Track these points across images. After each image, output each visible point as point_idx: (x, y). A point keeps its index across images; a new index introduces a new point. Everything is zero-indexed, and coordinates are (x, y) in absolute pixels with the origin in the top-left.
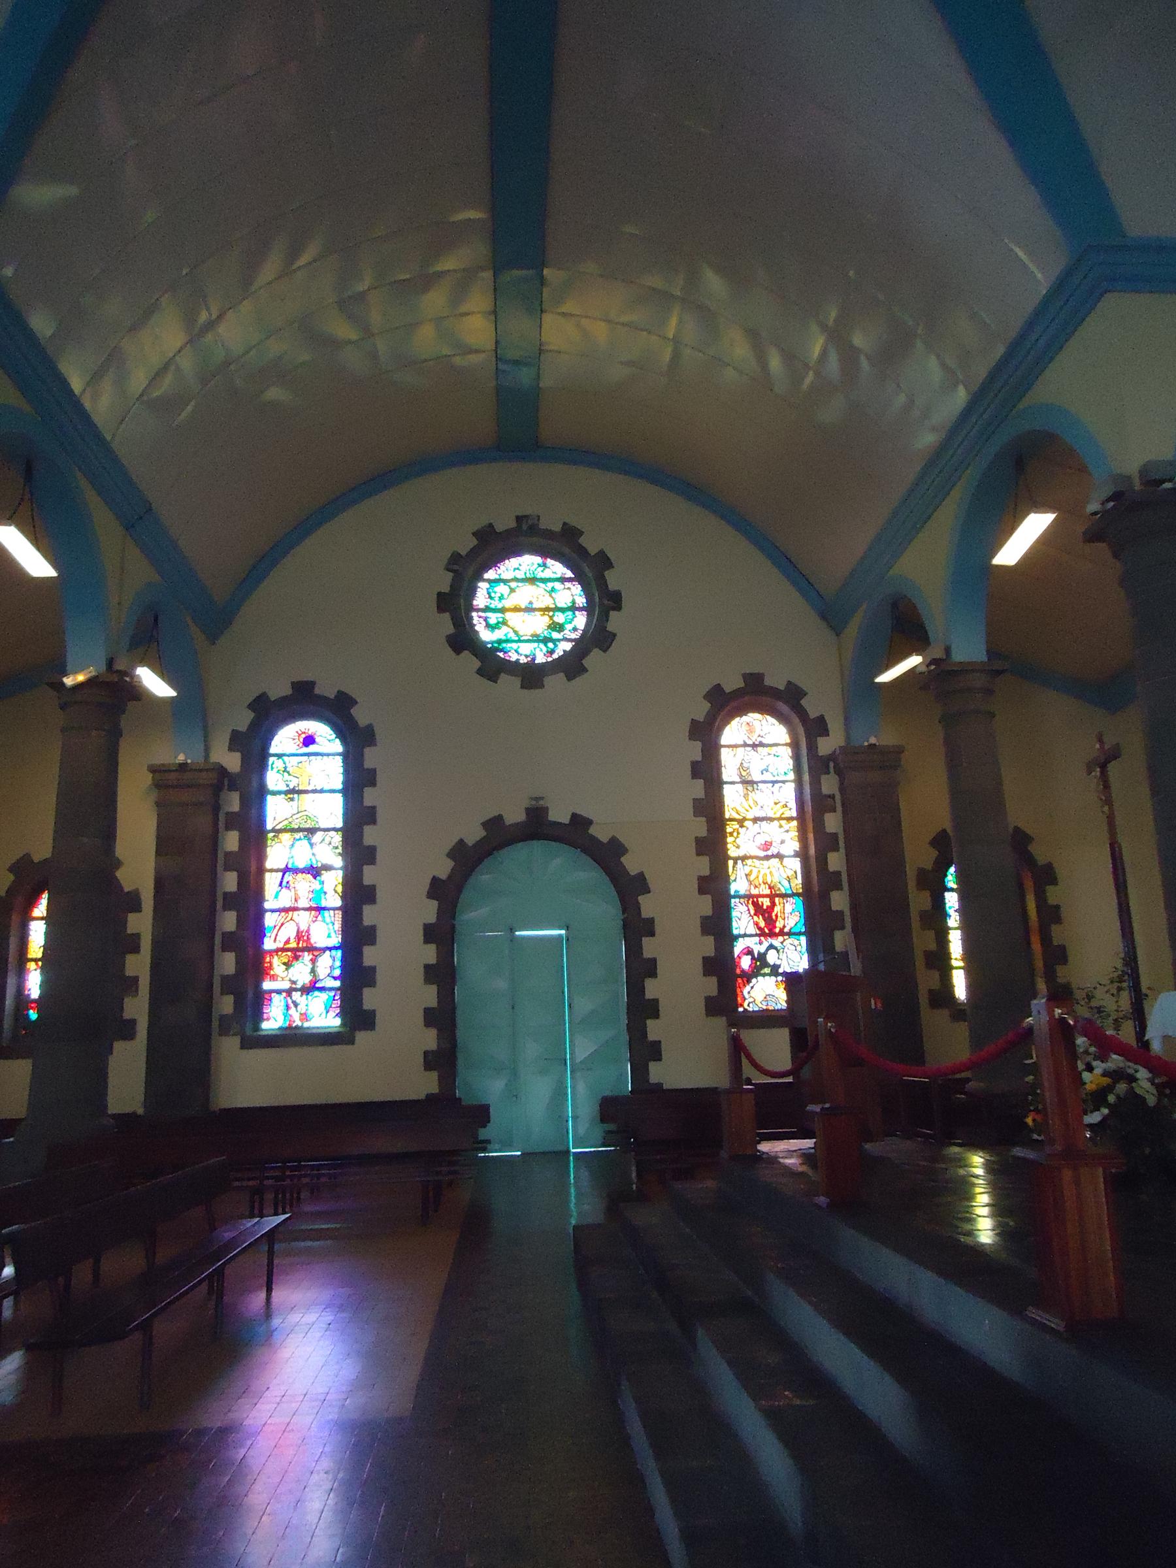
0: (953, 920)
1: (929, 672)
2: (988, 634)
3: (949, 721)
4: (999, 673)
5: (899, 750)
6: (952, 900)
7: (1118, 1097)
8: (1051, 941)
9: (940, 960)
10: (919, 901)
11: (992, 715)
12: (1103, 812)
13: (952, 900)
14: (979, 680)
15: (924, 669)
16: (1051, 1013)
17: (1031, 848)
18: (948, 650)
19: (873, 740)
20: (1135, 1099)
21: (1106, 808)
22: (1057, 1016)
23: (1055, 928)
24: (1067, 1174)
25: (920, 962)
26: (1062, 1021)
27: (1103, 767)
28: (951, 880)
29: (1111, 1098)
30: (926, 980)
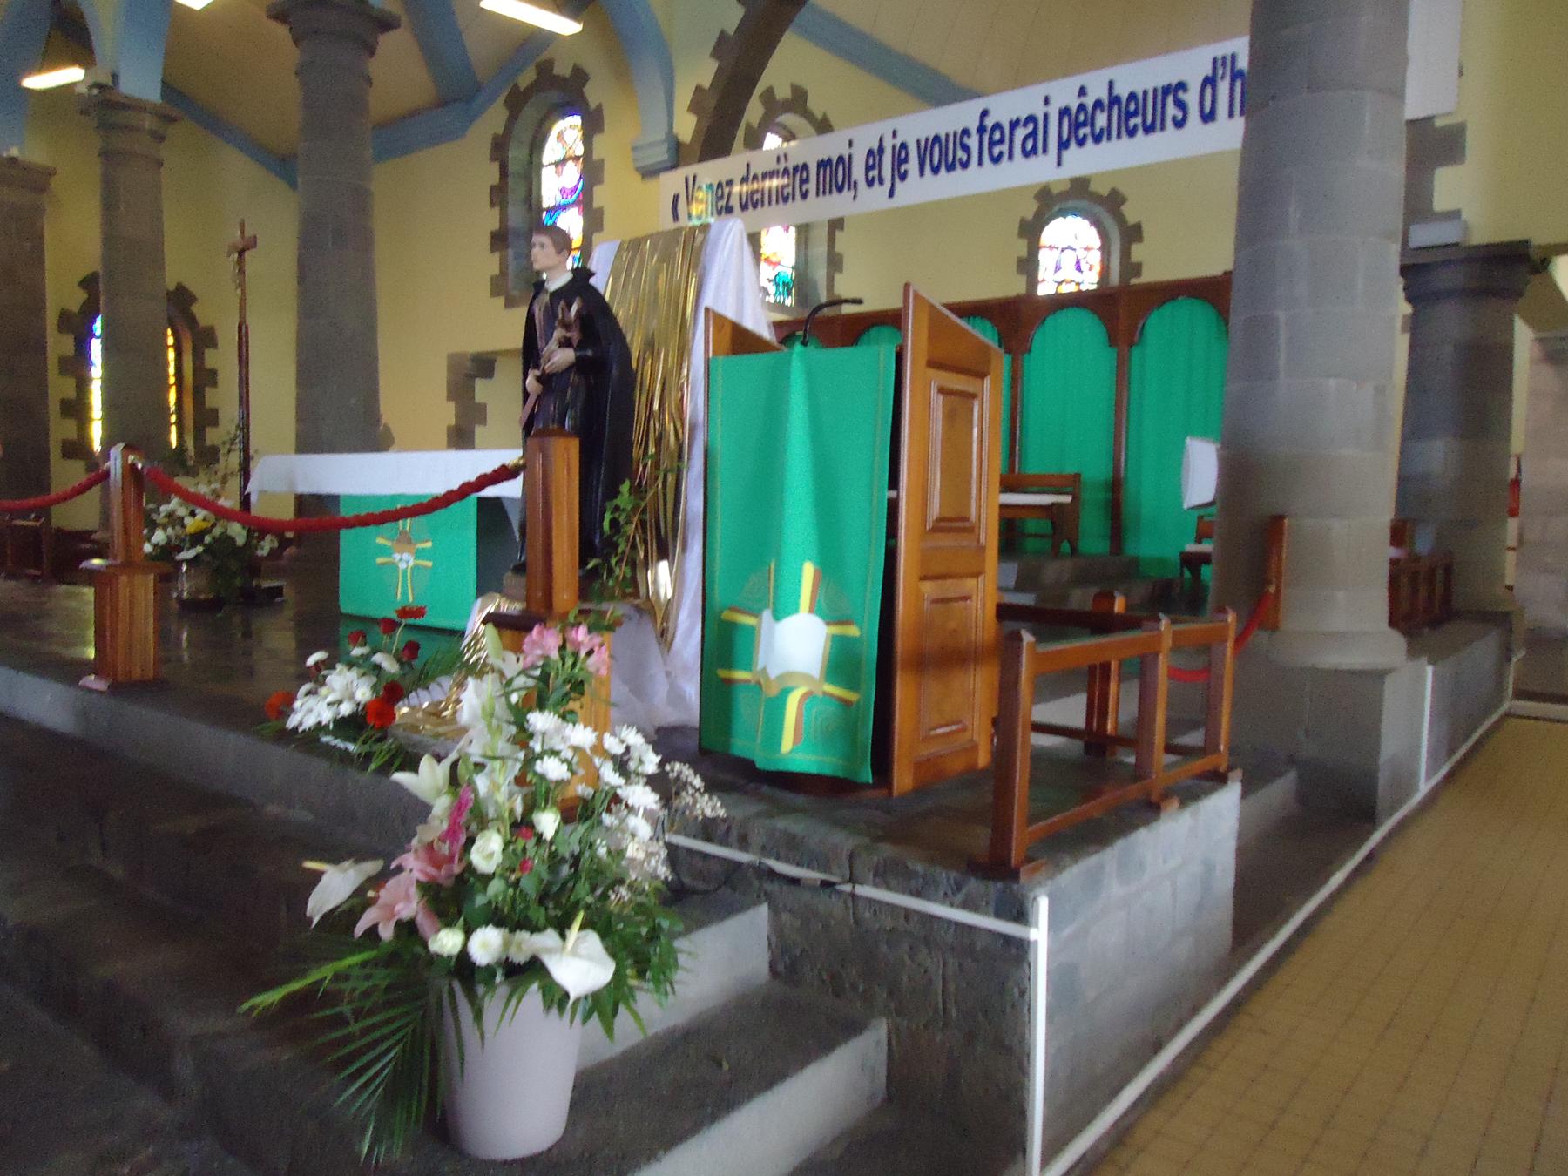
0: (97, 372)
1: (90, 97)
2: (165, 70)
3: (108, 156)
4: (172, 120)
5: (49, 173)
6: (96, 347)
7: (214, 538)
8: (203, 403)
9: (77, 409)
10: (59, 345)
11: (161, 164)
12: (237, 295)
13: (96, 347)
14: (148, 123)
15: (83, 90)
16: (125, 458)
17: (195, 309)
18: (115, 77)
19: (14, 152)
20: (227, 539)
21: (239, 291)
22: (129, 462)
23: (209, 392)
24: (123, 579)
25: (54, 408)
26: (133, 466)
27: (241, 253)
28: (98, 327)
29: (207, 539)
30: (62, 430)
